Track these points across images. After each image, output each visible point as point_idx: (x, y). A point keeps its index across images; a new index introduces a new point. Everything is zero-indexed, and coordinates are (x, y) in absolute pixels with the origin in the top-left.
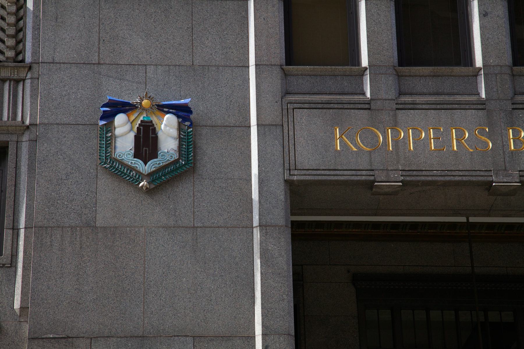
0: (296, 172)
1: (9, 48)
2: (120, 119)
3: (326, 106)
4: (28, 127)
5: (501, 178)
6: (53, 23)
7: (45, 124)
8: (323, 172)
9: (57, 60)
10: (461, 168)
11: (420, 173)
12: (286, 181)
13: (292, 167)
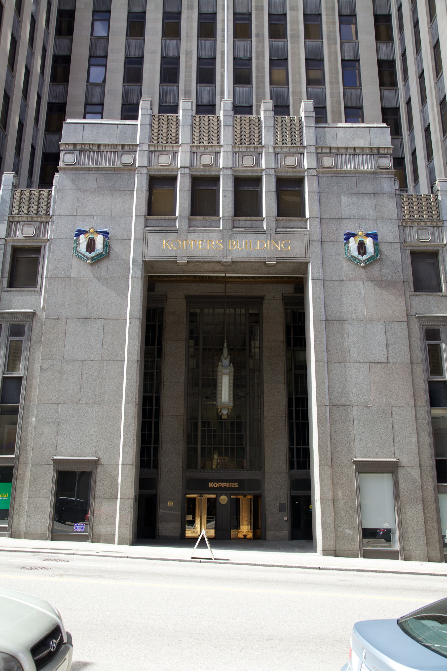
0: (147, 257)
1: (35, 210)
2: (82, 236)
3: (161, 231)
4: (49, 240)
5: (225, 260)
6: (61, 200)
7: (55, 239)
8: (157, 257)
9: (61, 214)
10: (210, 256)
11: (194, 258)
12: (143, 261)
13: (146, 255)
